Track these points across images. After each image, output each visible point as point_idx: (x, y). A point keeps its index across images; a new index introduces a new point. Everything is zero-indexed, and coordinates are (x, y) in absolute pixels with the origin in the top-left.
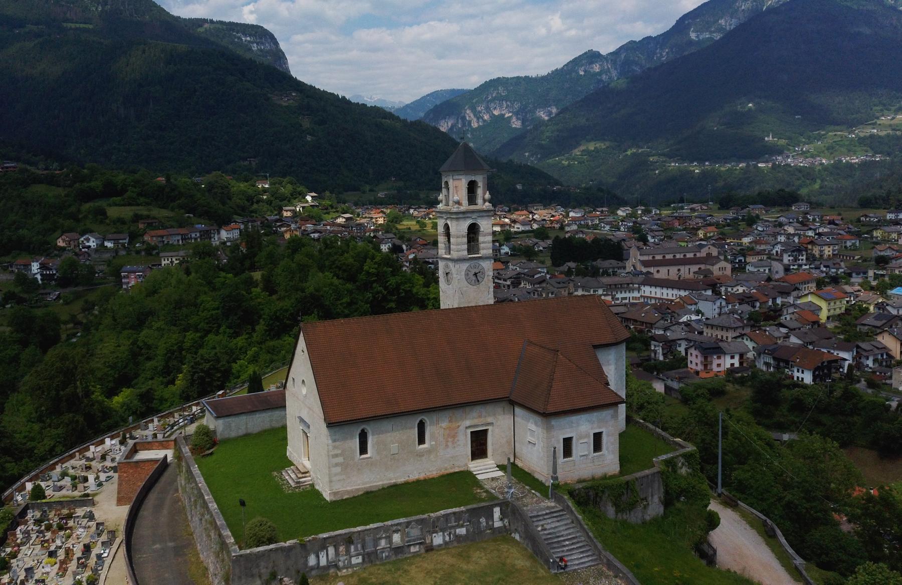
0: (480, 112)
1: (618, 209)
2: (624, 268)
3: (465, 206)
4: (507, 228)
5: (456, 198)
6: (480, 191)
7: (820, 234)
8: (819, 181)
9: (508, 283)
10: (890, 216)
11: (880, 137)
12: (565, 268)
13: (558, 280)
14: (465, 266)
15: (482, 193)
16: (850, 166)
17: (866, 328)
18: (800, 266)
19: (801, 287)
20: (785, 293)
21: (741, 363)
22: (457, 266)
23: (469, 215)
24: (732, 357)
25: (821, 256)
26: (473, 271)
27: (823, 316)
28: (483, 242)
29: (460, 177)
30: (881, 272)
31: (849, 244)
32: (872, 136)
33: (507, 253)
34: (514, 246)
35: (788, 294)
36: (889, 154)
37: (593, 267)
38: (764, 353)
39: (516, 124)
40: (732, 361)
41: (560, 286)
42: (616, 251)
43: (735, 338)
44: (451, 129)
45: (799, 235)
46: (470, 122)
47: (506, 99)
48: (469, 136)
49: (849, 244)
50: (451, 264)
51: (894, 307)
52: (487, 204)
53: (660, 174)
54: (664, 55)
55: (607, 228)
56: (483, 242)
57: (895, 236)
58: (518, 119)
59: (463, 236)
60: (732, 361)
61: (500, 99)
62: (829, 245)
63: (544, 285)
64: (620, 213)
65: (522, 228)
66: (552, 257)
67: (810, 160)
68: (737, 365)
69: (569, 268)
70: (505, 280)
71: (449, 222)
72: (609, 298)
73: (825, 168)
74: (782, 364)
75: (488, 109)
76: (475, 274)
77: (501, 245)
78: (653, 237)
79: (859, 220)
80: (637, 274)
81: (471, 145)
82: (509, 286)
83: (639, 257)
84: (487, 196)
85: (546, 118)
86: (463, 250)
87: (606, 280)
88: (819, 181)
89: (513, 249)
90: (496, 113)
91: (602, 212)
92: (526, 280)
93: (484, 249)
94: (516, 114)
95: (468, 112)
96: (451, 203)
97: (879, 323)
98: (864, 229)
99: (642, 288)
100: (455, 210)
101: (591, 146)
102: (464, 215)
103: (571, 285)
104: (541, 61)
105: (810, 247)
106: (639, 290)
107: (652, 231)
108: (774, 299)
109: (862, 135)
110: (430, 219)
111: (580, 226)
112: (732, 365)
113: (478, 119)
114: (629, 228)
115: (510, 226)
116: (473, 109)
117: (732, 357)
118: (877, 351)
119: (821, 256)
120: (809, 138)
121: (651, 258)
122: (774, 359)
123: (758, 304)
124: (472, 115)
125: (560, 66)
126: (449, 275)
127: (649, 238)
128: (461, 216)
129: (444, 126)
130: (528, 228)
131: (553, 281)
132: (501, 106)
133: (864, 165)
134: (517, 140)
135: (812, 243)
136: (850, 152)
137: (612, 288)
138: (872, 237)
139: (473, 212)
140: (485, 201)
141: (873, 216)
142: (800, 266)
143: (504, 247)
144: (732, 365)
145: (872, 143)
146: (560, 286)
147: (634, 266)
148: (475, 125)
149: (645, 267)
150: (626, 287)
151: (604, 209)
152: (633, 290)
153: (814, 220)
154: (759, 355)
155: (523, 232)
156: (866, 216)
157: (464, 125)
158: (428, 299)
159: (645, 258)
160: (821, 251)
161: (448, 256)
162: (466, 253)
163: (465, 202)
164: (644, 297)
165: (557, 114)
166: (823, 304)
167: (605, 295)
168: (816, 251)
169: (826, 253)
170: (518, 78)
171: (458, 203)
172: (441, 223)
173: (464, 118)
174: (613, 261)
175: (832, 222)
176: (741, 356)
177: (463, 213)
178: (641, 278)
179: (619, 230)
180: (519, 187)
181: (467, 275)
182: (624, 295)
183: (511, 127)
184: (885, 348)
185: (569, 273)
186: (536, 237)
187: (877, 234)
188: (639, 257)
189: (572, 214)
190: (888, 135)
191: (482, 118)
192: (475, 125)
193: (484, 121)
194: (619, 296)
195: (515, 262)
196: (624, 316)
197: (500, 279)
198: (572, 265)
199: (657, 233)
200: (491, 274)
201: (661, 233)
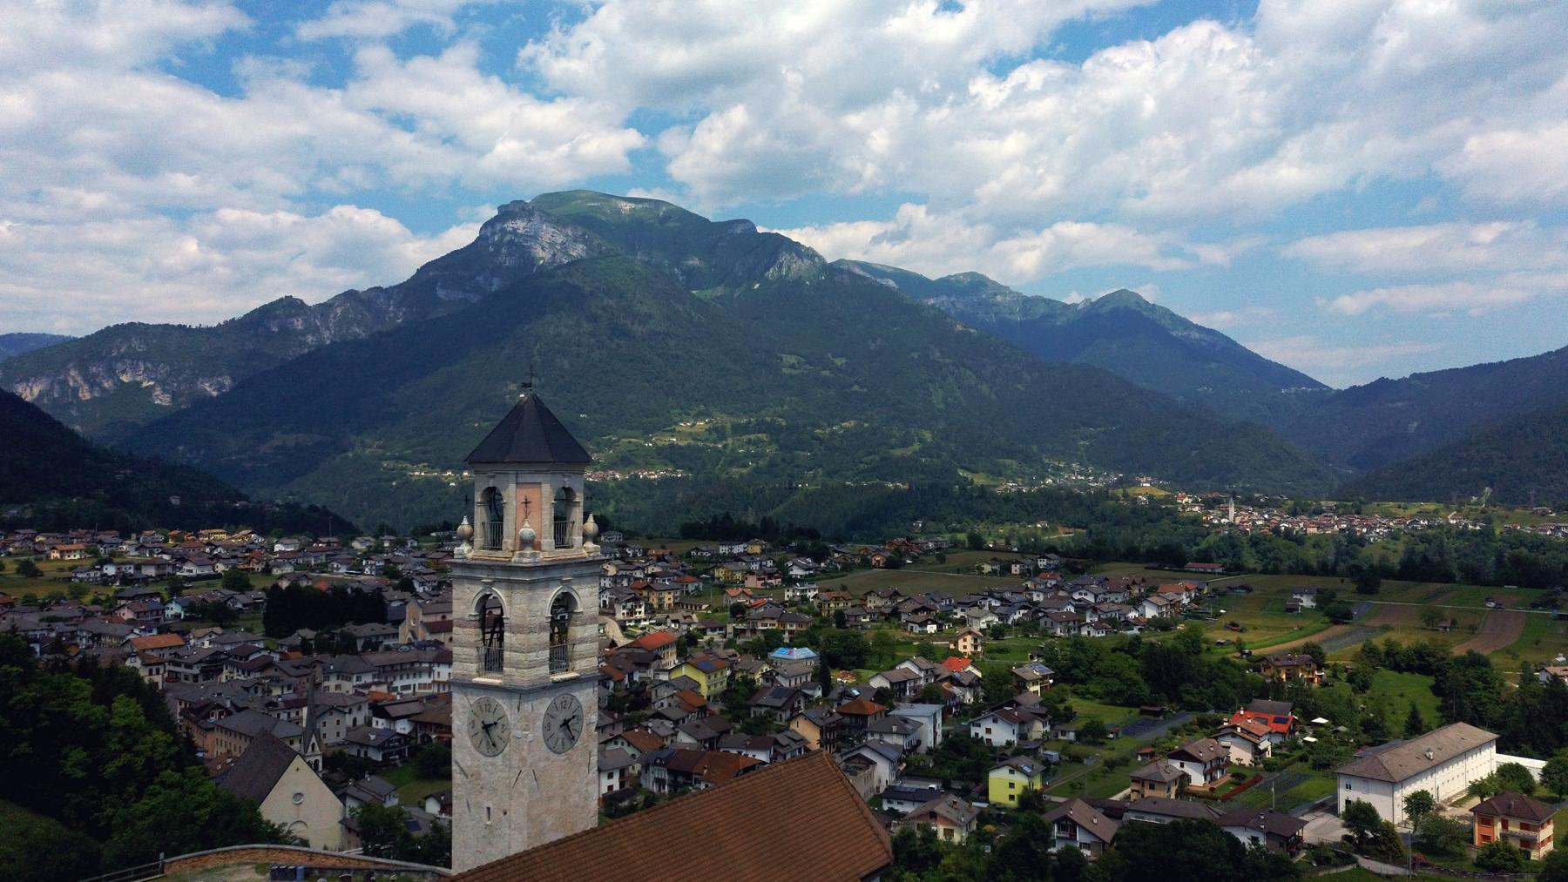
0: (95, 376)
1: (353, 539)
2: (396, 635)
3: (548, 552)
4: (169, 570)
5: (527, 530)
6: (577, 514)
7: (653, 575)
8: (613, 503)
9: (196, 671)
10: (723, 549)
11: (681, 448)
12: (295, 639)
13: (297, 663)
14: (542, 705)
15: (582, 524)
16: (649, 483)
17: (763, 710)
18: (638, 621)
19: (661, 653)
20: (644, 665)
21: (622, 784)
22: (527, 707)
23: (555, 574)
24: (610, 776)
25: (661, 606)
26: (562, 716)
27: (704, 691)
28: (582, 641)
29: (538, 478)
30: (740, 626)
31: (691, 588)
32: (672, 446)
33: (177, 616)
34: (192, 603)
35: (646, 666)
36: (691, 470)
37: (344, 636)
38: (655, 764)
39: (162, 399)
40: (611, 782)
41: (299, 672)
42: (372, 607)
43: (605, 743)
44: (41, 395)
45: (629, 578)
46: (75, 390)
47: (145, 357)
48: (74, 412)
49: (691, 588)
50: (505, 705)
51: (785, 677)
52: (590, 545)
53: (397, 487)
54: (397, 317)
55: (343, 570)
56: (582, 641)
57: (739, 576)
58: (164, 391)
59: (542, 629)
60: (611, 782)
61: (134, 358)
62: (669, 590)
63: (271, 672)
64: (356, 545)
65: (196, 571)
66: (267, 621)
67: (600, 473)
68: (616, 788)
69: (304, 639)
70: (189, 666)
71: (500, 593)
72: (383, 689)
73: (620, 485)
74: (680, 779)
75: (111, 372)
76: (566, 723)
77: (164, 603)
78: (422, 584)
79: (689, 555)
80: (423, 646)
81: (77, 428)
82: (196, 677)
83: (421, 618)
84: (591, 526)
85: (215, 394)
86: (541, 664)
87: (377, 658)
88: (613, 503)
89: (190, 607)
90: (125, 378)
91: (329, 543)
92: (233, 665)
93: (583, 657)
94: (162, 383)
95: (73, 373)
96: (508, 542)
97: (779, 703)
98: (700, 567)
99: (436, 669)
100: (527, 561)
101: (290, 440)
102: (512, 575)
103: (319, 669)
104: (210, 306)
105: (645, 593)
106: (430, 672)
107: (419, 574)
108: (631, 675)
109: (660, 443)
110: (9, 554)
111: (297, 566)
112: (610, 788)
113: (92, 386)
114: (378, 569)
115: (174, 567)
116: (83, 369)
117: (610, 776)
118: (794, 746)
119: (661, 606)
120: (598, 444)
121: (439, 618)
122: (670, 772)
123: (612, 684)
124: (79, 379)
125: (238, 316)
126: (496, 732)
127: (416, 585)
128: (539, 576)
129: (30, 392)
130: (207, 571)
131: (286, 666)
132: (135, 369)
133: (664, 481)
134: (167, 423)
135: (648, 588)
136: (648, 465)
137: (387, 672)
138: (713, 578)
139: (491, 568)
140: (586, 537)
141: (705, 550)
142: (638, 621)
143: (173, 605)
144: (610, 788)
145: (671, 455)
146: (299, 672)
147: (413, 633)
148: (85, 395)
149: (432, 632)
150: (410, 668)
151: (333, 539)
152: (419, 673)
153: (635, 555)
154: (646, 767)
155: (199, 578)
156: (698, 550)
157: (63, 394)
158: (108, 727)
159: (432, 619)
160: (660, 599)
161: (493, 680)
162: (545, 670)
163: (548, 541)
164: (439, 683)
165: (234, 389)
166: (701, 679)
167: (377, 684)
168: (654, 601)
169: (667, 602)
170: (166, 326)
171: (525, 543)
172: (464, 601)
173: (64, 383)
174: (374, 625)
175: (660, 559)
176: (622, 772)
177: (545, 568)
178: (431, 653)
179: (362, 572)
180: (175, 501)
181: (547, 727)
182: (406, 682)
183: (151, 404)
184: (803, 739)
185: (305, 647)
186: (227, 586)
187: (720, 573)
188: (421, 618)
189: (278, 548)
190: (689, 446)
191: (100, 385)
192: (85, 395)
193: (104, 390)
194: (398, 683)
195: (200, 632)
196: (420, 719)
197: (178, 665)
198: (308, 633)
199: (427, 578)
200: (594, 718)
201: (434, 577)
